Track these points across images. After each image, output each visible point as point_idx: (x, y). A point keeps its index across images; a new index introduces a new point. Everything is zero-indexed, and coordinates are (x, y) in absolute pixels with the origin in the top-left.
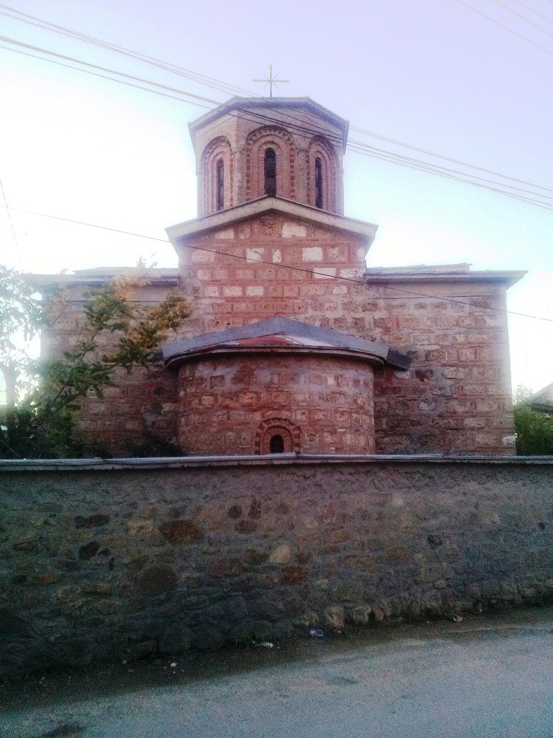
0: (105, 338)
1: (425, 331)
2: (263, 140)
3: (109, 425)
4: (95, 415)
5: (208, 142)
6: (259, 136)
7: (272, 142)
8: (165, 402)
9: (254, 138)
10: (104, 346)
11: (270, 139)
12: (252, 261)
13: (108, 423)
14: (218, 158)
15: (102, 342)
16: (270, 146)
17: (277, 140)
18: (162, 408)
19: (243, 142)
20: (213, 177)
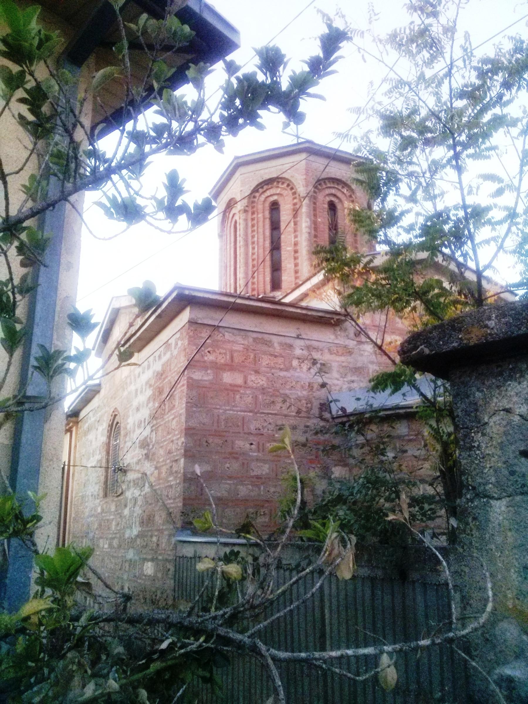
0: (264, 379)
1: (190, 614)
2: (328, 191)
3: (274, 492)
4: (258, 477)
5: (261, 180)
6: (324, 186)
7: (335, 195)
8: (336, 465)
9: (319, 187)
10: (263, 389)
11: (333, 191)
12: (29, 376)
13: (272, 490)
14: (272, 199)
15: (261, 383)
16: (333, 199)
17: (339, 194)
18: (332, 473)
19: (311, 188)
20: (264, 218)
